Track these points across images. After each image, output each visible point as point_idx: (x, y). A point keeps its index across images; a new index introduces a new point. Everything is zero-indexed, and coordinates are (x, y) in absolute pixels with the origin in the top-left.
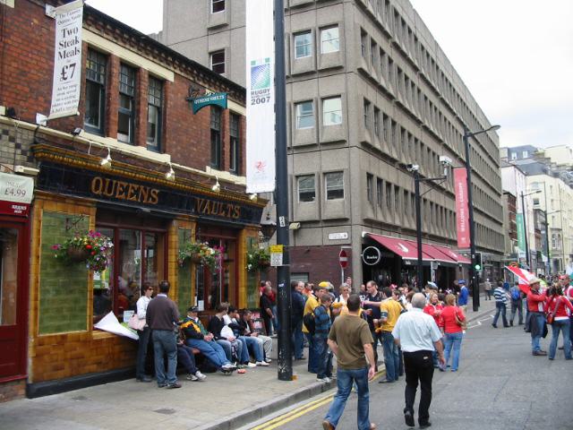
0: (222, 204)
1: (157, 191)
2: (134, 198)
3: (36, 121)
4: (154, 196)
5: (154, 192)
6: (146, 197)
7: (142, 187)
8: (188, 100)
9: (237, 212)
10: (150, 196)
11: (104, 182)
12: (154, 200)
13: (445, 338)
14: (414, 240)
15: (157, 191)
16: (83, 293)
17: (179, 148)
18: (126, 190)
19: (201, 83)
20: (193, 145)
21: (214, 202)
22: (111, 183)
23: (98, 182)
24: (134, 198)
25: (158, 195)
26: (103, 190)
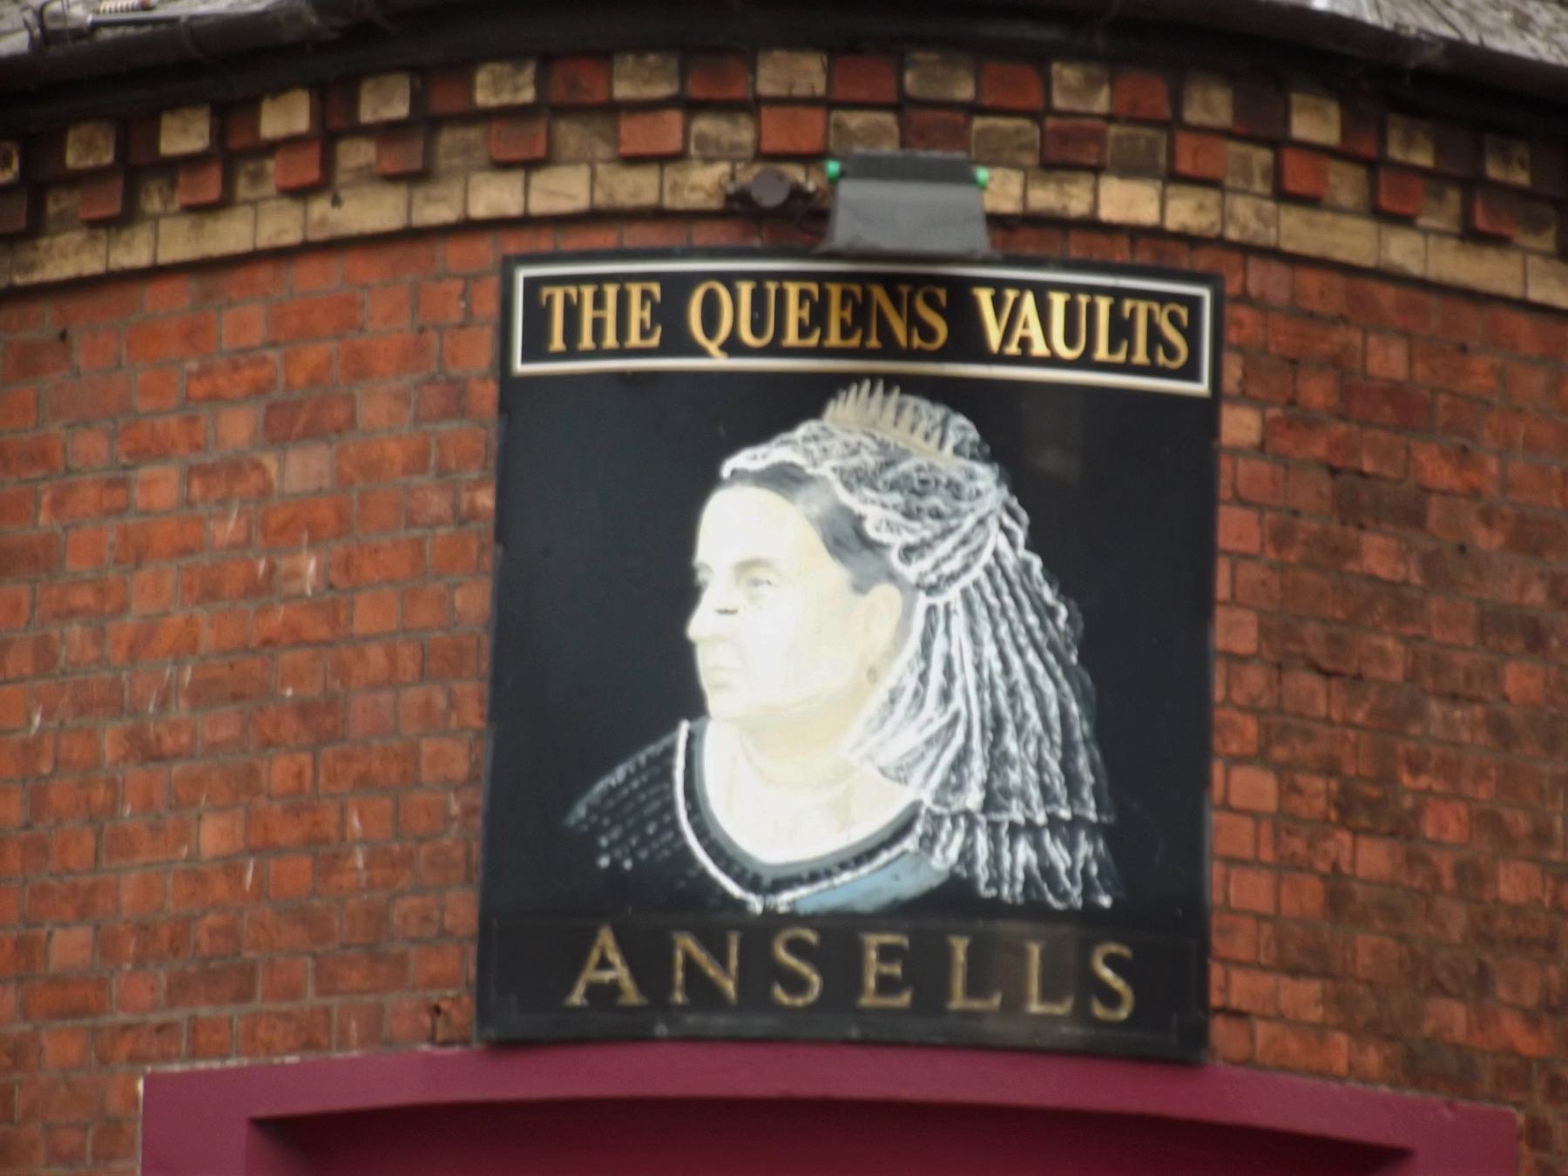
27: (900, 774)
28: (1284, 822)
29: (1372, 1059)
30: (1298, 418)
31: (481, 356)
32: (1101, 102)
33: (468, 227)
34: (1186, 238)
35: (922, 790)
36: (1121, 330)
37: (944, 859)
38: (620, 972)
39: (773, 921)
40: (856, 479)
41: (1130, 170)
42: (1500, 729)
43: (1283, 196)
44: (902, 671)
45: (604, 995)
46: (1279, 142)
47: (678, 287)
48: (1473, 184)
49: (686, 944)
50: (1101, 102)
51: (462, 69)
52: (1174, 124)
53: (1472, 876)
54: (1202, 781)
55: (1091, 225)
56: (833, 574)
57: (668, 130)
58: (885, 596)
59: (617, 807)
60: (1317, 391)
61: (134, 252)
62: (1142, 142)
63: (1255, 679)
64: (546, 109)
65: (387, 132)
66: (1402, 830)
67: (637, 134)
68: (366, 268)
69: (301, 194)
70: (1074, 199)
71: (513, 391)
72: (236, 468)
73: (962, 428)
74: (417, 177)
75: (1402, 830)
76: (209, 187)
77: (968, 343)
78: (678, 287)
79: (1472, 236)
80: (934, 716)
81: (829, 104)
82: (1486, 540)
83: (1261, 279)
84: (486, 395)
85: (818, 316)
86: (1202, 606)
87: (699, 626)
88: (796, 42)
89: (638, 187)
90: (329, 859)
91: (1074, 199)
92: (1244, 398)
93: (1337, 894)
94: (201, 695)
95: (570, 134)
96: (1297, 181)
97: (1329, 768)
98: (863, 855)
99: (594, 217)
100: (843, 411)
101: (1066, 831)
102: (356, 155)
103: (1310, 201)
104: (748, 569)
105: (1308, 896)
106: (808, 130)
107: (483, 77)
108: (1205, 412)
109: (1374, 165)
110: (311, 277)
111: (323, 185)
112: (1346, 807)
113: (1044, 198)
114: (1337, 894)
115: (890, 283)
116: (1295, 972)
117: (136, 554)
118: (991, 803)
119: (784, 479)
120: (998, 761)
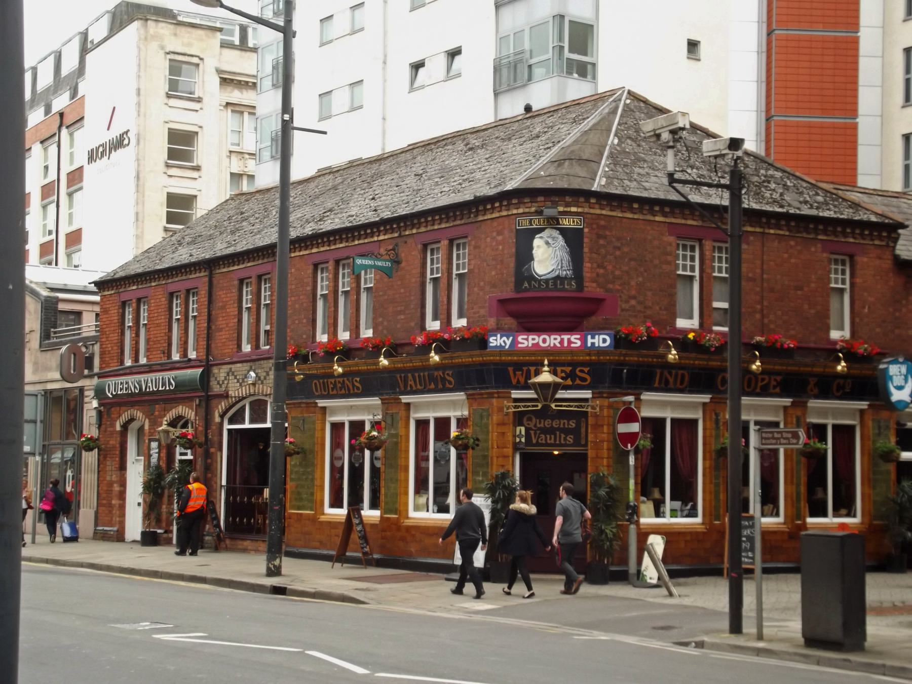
0: (426, 374)
1: (450, 373)
2: (343, 391)
3: (855, 182)
4: (358, 385)
5: (356, 381)
6: (351, 387)
7: (345, 379)
8: (395, 262)
9: (358, 385)
10: (353, 385)
11: (319, 382)
12: (358, 388)
13: (108, 446)
14: (214, 402)
15: (358, 379)
16: (386, 503)
17: (385, 323)
18: (335, 385)
19: (407, 233)
20: (400, 313)
21: (417, 375)
22: (419, 376)
23: (315, 383)
24: (343, 391)
25: (360, 382)
26: (321, 391)
27: (553, 265)
28: (592, 268)
29: (602, 290)
30: (592, 229)
31: (514, 227)
32: (571, 200)
33: (513, 215)
34: (580, 213)
35: (555, 267)
36: (573, 222)
37: (557, 273)
38: (527, 285)
39: (541, 280)
40: (548, 237)
41: (574, 206)
42: (615, 258)
43: (590, 208)
44: (553, 255)
45: (526, 287)
46: (590, 203)
47: (531, 220)
48: (611, 205)
49: (533, 282)
50: (571, 200)
51: (511, 199)
52: (578, 202)
53: (613, 272)
54: (583, 264)
55: (570, 212)
56: (545, 246)
57: (530, 205)
58: (551, 248)
59: (527, 269)
60: (594, 226)
61: (486, 218)
62: (628, 101)
63: (588, 254)
64: (519, 203)
65: (505, 206)
66: (605, 268)
67: (527, 205)
68: (504, 218)
69: (499, 212)
70: (568, 209)
71: (517, 230)
72: (495, 238)
73: (558, 232)
74: (508, 210)
75: (605, 268)
76: (491, 211)
77: (558, 223)
78: (531, 219)
79: (611, 210)
80: (556, 260)
81: (544, 201)
82: (614, 240)
83: (588, 216)
84: (514, 230)
85: (544, 222)
86: (582, 247)
87: (534, 252)
88: (541, 196)
89: (527, 210)
90: (502, 274)
91: (568, 209)
92: (587, 227)
93: (598, 275)
94: (493, 259)
95: (521, 205)
96: (591, 205)
97: (596, 262)
98: (549, 273)
99: (523, 213)
100: (547, 231)
101: (569, 270)
102: (503, 208)
103: (593, 208)
104: (538, 247)
105: (594, 275)
106: (542, 204)
107: (465, 325)
108: (582, 229)
109: (600, 204)
110: (500, 219)
111: (500, 211)
112: (599, 266)
113: (565, 209)
114: (598, 275)
115: (551, 218)
116: (593, 282)
117: (486, 247)
118: (562, 267)
119: (541, 237)
120: (562, 264)
